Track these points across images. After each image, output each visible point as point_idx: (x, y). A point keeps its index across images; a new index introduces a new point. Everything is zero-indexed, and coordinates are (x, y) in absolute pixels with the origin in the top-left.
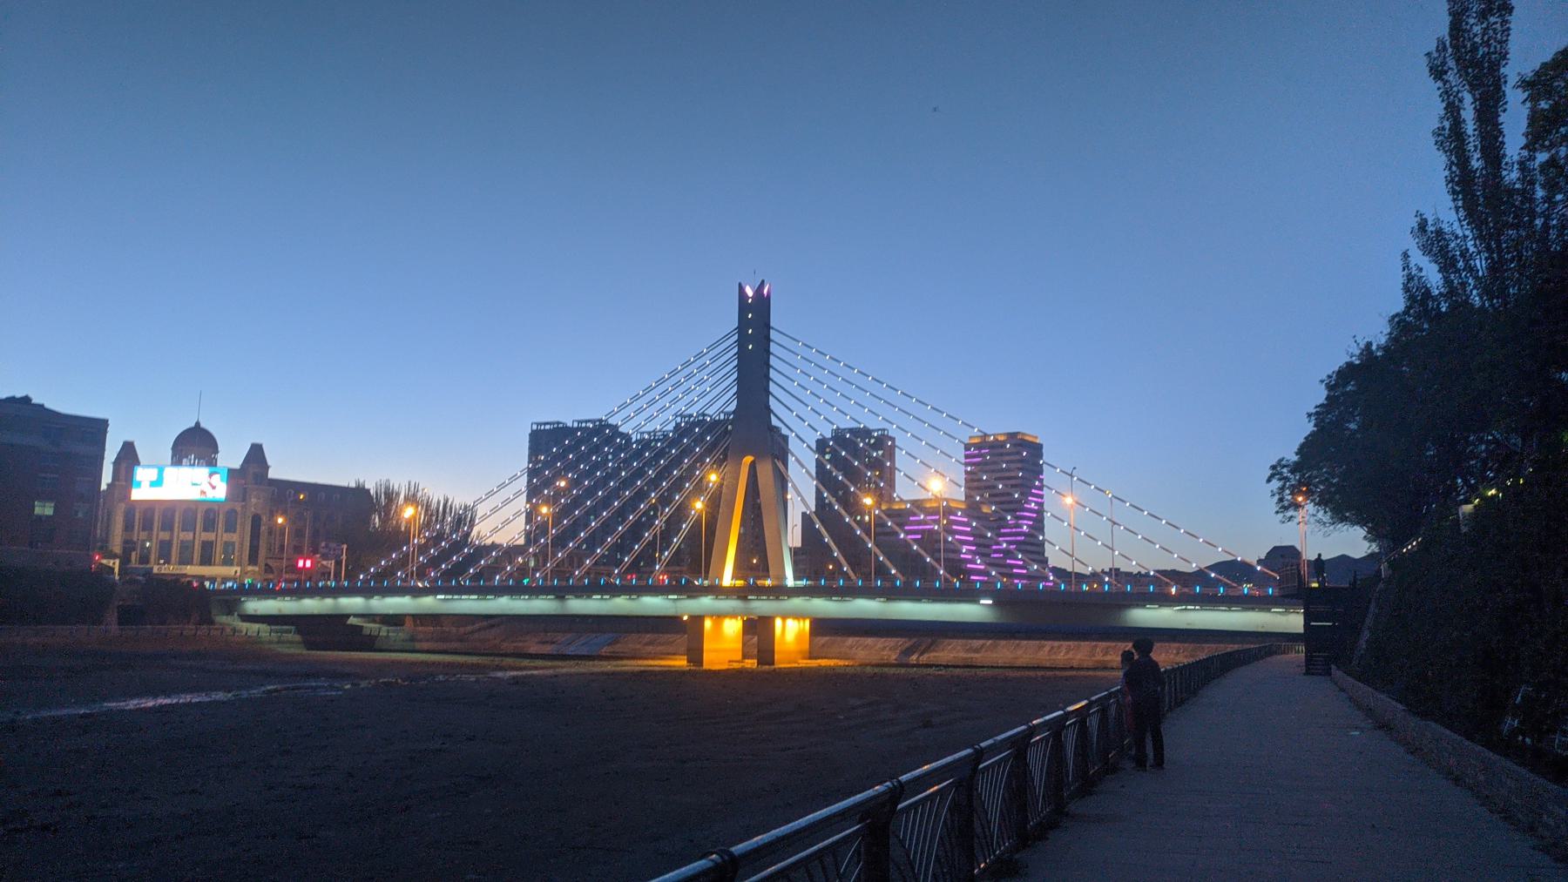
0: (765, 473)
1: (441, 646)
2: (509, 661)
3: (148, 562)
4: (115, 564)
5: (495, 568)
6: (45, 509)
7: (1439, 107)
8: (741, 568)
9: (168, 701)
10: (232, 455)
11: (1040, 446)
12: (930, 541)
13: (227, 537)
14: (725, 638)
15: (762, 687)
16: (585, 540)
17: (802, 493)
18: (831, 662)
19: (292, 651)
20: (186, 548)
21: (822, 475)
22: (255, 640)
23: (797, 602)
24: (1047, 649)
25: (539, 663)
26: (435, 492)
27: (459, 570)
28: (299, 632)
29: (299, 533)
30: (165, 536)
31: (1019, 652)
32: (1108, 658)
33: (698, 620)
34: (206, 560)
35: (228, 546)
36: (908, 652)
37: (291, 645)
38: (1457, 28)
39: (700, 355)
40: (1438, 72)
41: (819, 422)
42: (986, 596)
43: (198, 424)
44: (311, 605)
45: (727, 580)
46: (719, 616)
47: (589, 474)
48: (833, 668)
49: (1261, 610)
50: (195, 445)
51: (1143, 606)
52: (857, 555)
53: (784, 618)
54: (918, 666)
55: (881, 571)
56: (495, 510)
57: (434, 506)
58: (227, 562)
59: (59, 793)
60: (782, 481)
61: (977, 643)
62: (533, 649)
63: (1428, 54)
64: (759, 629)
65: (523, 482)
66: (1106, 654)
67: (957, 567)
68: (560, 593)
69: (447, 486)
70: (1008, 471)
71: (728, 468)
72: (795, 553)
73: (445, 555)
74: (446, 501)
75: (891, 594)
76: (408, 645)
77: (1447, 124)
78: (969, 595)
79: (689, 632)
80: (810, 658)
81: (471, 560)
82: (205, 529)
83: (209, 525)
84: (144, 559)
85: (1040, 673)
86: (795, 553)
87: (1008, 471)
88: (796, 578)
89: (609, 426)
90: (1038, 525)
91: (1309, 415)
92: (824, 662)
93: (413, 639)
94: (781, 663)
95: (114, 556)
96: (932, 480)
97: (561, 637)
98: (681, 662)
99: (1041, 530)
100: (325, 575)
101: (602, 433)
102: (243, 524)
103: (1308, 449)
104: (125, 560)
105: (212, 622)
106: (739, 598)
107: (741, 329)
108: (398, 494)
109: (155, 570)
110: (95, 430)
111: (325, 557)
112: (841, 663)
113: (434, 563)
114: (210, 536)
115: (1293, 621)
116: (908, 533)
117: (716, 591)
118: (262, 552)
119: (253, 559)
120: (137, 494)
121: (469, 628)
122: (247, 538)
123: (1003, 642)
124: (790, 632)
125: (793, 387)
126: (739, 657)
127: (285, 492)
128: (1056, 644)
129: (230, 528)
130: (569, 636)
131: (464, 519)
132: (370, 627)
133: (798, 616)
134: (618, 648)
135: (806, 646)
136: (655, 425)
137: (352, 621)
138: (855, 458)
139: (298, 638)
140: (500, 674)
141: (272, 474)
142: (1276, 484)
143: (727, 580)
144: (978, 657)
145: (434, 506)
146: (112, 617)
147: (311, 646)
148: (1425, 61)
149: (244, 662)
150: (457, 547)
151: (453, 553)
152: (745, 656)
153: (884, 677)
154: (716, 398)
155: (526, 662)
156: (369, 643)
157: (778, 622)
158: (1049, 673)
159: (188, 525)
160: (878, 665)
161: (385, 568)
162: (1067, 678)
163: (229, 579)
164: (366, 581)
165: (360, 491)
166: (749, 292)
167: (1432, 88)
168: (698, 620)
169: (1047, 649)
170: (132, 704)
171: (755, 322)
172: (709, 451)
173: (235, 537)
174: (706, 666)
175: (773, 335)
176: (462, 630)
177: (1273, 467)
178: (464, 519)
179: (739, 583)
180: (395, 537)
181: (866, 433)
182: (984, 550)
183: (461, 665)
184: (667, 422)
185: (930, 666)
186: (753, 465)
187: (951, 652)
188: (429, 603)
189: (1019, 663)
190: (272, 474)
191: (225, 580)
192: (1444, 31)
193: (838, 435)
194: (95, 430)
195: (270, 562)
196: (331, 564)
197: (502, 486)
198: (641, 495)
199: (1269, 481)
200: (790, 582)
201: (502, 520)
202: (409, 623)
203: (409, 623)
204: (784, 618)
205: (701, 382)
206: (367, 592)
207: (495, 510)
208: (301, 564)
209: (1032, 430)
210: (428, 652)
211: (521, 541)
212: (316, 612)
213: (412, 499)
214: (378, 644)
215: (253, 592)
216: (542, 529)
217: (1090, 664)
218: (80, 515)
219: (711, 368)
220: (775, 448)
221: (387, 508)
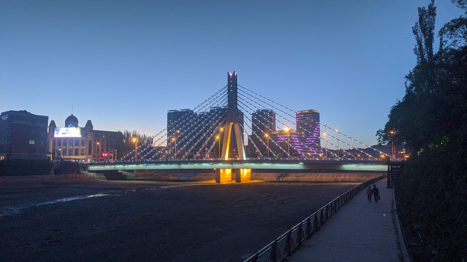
0: (237, 127)
2: (165, 182)
3: (60, 155)
4: (51, 156)
5: (160, 155)
6: (32, 142)
7: (415, 42)
9: (74, 199)
10: (82, 124)
11: (319, 114)
12: (284, 145)
13: (82, 147)
14: (226, 174)
15: (237, 189)
16: (185, 147)
17: (248, 131)
19: (102, 181)
20: (71, 151)
21: (254, 128)
22: (93, 178)
23: (247, 164)
24: (320, 176)
25: (174, 183)
26: (141, 133)
28: (105, 175)
29: (102, 146)
30: (64, 147)
33: (218, 170)
34: (77, 154)
36: (279, 177)
37: (102, 179)
38: (421, 20)
40: (415, 32)
41: (252, 107)
43: (72, 115)
44: (108, 167)
45: (227, 158)
46: (224, 169)
47: (186, 128)
48: (257, 183)
50: (72, 121)
51: (347, 164)
52: (263, 149)
53: (243, 169)
55: (271, 155)
56: (159, 139)
57: (141, 137)
58: (83, 154)
59: (57, 230)
60: (242, 130)
61: (299, 174)
62: (172, 178)
63: (413, 28)
64: (236, 172)
65: (166, 132)
68: (179, 163)
70: (309, 121)
71: (226, 126)
72: (246, 147)
73: (145, 152)
75: (273, 162)
76: (136, 178)
77: (417, 47)
78: (296, 162)
80: (251, 179)
81: (153, 153)
83: (77, 144)
84: (59, 154)
85: (317, 184)
86: (246, 147)
87: (309, 121)
92: (255, 181)
93: (137, 176)
94: (243, 181)
95: (50, 154)
96: (286, 126)
97: (179, 174)
98: (214, 182)
99: (319, 136)
100: (111, 157)
101: (188, 113)
103: (389, 127)
104: (54, 154)
105: (80, 173)
106: (230, 163)
107: (229, 85)
108: (130, 134)
111: (110, 153)
113: (142, 154)
114: (77, 147)
117: (224, 162)
118: (92, 151)
119: (90, 154)
120: (56, 136)
122: (88, 146)
123: (307, 174)
124: (245, 173)
126: (230, 180)
127: (99, 134)
128: (322, 174)
129: (83, 145)
131: (150, 141)
133: (247, 168)
135: (250, 176)
138: (264, 119)
139: (104, 177)
140: (163, 187)
141: (94, 129)
142: (378, 137)
143: (227, 158)
145: (141, 137)
146: (52, 172)
148: (412, 29)
149: (92, 186)
150: (148, 150)
151: (147, 151)
152: (232, 179)
153: (272, 186)
154: (222, 103)
155: (170, 183)
157: (241, 170)
161: (128, 156)
162: (326, 185)
163: (83, 159)
164: (123, 160)
165: (120, 133)
166: (231, 75)
167: (414, 36)
168: (218, 170)
169: (320, 176)
170: (64, 200)
171: (233, 83)
172: (221, 120)
174: (221, 183)
177: (378, 132)
178: (150, 141)
179: (230, 159)
180: (131, 147)
181: (267, 111)
183: (151, 185)
184: (207, 109)
186: (233, 125)
187: (291, 177)
188: (141, 166)
190: (94, 129)
191: (82, 160)
192: (418, 20)
193: (258, 111)
196: (112, 155)
197: (161, 132)
198: (201, 135)
203: (135, 172)
204: (243, 169)
206: (124, 164)
207: (159, 139)
208: (104, 155)
209: (316, 109)
213: (135, 136)
214: (127, 178)
215: (92, 164)
216: (173, 144)
218: (42, 144)
219: (220, 97)
221: (127, 138)
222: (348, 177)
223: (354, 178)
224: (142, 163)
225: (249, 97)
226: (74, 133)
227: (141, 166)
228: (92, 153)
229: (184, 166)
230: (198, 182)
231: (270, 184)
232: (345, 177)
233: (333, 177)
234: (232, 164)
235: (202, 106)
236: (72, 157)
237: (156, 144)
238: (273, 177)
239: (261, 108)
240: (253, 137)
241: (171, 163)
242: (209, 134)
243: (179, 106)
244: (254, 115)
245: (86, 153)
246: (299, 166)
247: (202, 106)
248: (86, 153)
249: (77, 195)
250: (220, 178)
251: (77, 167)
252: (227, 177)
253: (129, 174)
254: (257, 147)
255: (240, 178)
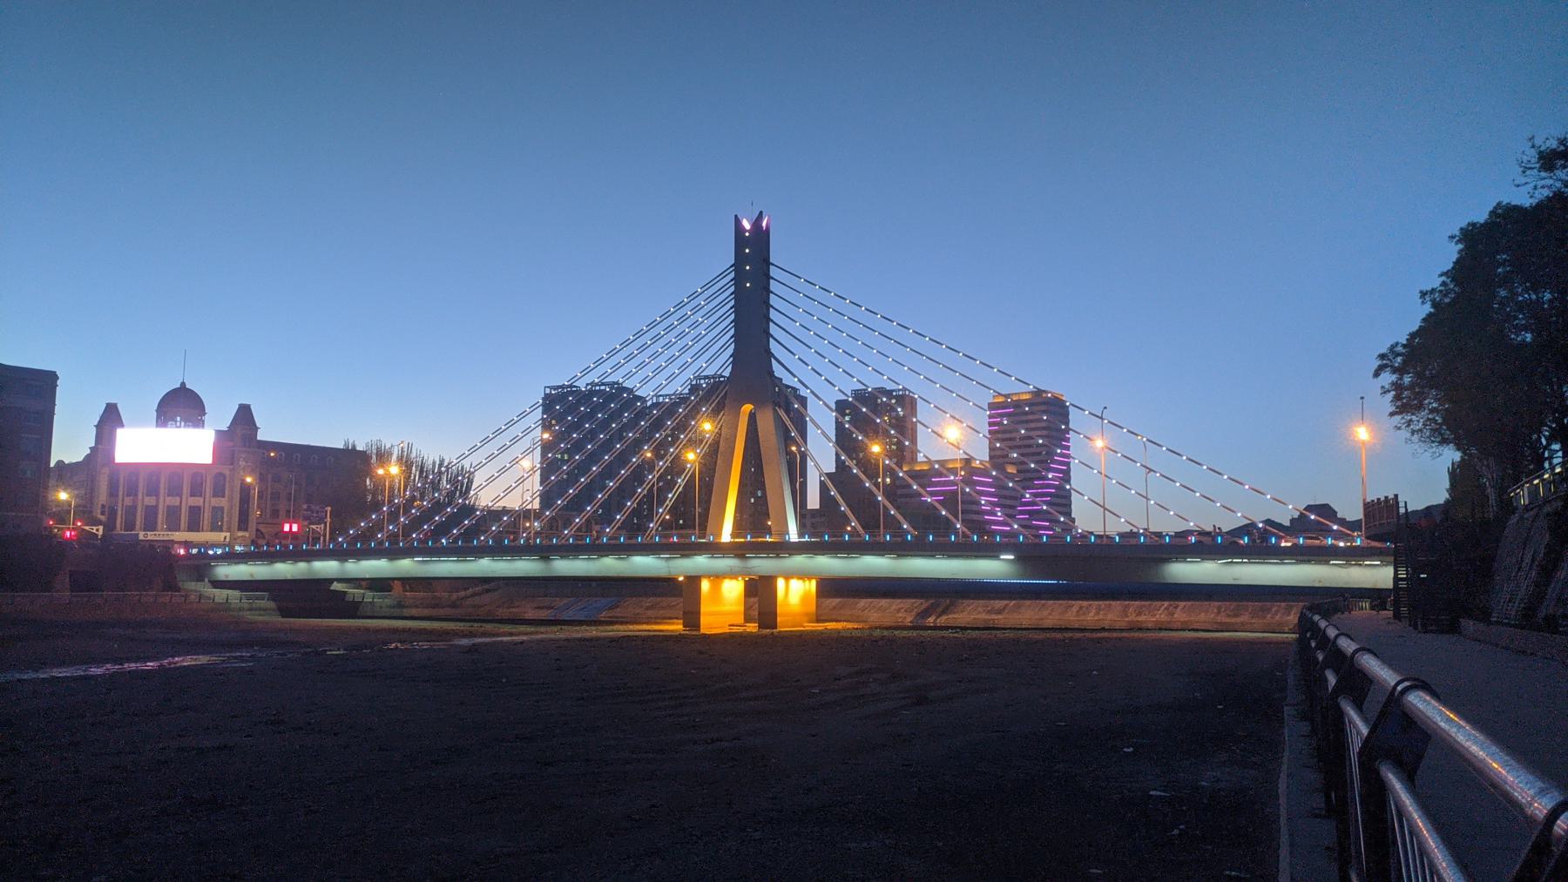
1: (426, 612)
8: (738, 529)
10: (220, 416)
13: (216, 502)
14: (724, 601)
18: (839, 626)
19: (266, 618)
20: (173, 513)
22: (225, 606)
23: (799, 560)
24: (1075, 609)
27: (442, 529)
30: (150, 501)
31: (1045, 613)
32: (1142, 618)
33: (694, 581)
34: (194, 526)
35: (217, 511)
36: (925, 614)
37: (264, 614)
39: (694, 296)
41: (837, 375)
42: (1007, 552)
43: (183, 384)
46: (717, 577)
47: (576, 426)
49: (1319, 562)
50: (181, 405)
54: (935, 628)
55: (893, 525)
58: (215, 528)
61: (999, 604)
62: (530, 615)
64: (760, 591)
66: (1139, 614)
67: (979, 527)
68: (544, 553)
69: (437, 446)
70: (1033, 430)
71: (724, 417)
74: (442, 462)
75: (901, 548)
76: (397, 612)
78: (988, 550)
79: (683, 594)
80: (818, 621)
82: (193, 495)
83: (196, 491)
84: (130, 526)
87: (1033, 430)
88: (801, 535)
89: (626, 389)
90: (1066, 477)
91: (1423, 294)
92: (831, 625)
93: (400, 605)
94: (784, 625)
95: (97, 522)
96: (952, 436)
98: (677, 627)
99: (1068, 481)
102: (232, 490)
104: (109, 526)
107: (738, 266)
109: (141, 537)
110: (41, 385)
112: (850, 625)
115: (1379, 575)
116: (932, 494)
117: (715, 549)
119: (243, 525)
121: (462, 594)
124: (795, 595)
125: (795, 328)
126: (741, 620)
128: (1085, 603)
129: (219, 492)
130: (566, 601)
132: (355, 592)
133: (803, 575)
134: (618, 612)
135: (813, 608)
136: (668, 390)
137: (336, 586)
138: (876, 413)
139: (272, 604)
141: (259, 437)
143: (726, 536)
144: (1000, 619)
147: (285, 612)
149: (211, 630)
151: (444, 512)
152: (748, 619)
153: (891, 641)
156: (351, 609)
157: (781, 582)
158: (1078, 635)
159: (175, 491)
160: (887, 628)
162: (1099, 641)
166: (747, 225)
168: (694, 581)
169: (1075, 609)
171: (753, 259)
173: (223, 502)
174: (703, 631)
175: (773, 272)
176: (455, 596)
177: (1382, 356)
178: (462, 483)
182: (1008, 502)
185: (947, 628)
186: (752, 416)
187: (970, 614)
188: (407, 566)
189: (1048, 623)
193: (860, 396)
194: (41, 385)
195: (261, 527)
199: (1377, 374)
200: (793, 535)
201: (510, 480)
202: (397, 586)
203: (397, 586)
204: (787, 578)
205: (695, 325)
206: (341, 555)
208: (287, 528)
209: (1053, 387)
210: (412, 618)
211: (536, 505)
212: (289, 577)
215: (231, 557)
217: (1123, 625)
220: (788, 406)
222: (1181, 612)
223: (1202, 617)
224: (409, 552)
225: (814, 307)
226: (192, 446)
227: (407, 566)
228: (253, 525)
229: (565, 567)
230: (616, 627)
231: (886, 633)
232: (1172, 614)
233: (1125, 613)
234: (742, 556)
235: (639, 343)
236: (178, 536)
237: (485, 496)
238: (897, 612)
239: (873, 383)
240: (840, 476)
241: (516, 551)
242: (659, 452)
243: (577, 368)
244: (841, 407)
245: (229, 522)
246: (995, 568)
247: (639, 343)
248: (229, 522)
249: (72, 664)
250: (698, 613)
251: (161, 568)
252: (726, 608)
253: (369, 596)
254: (849, 513)
255: (775, 614)
